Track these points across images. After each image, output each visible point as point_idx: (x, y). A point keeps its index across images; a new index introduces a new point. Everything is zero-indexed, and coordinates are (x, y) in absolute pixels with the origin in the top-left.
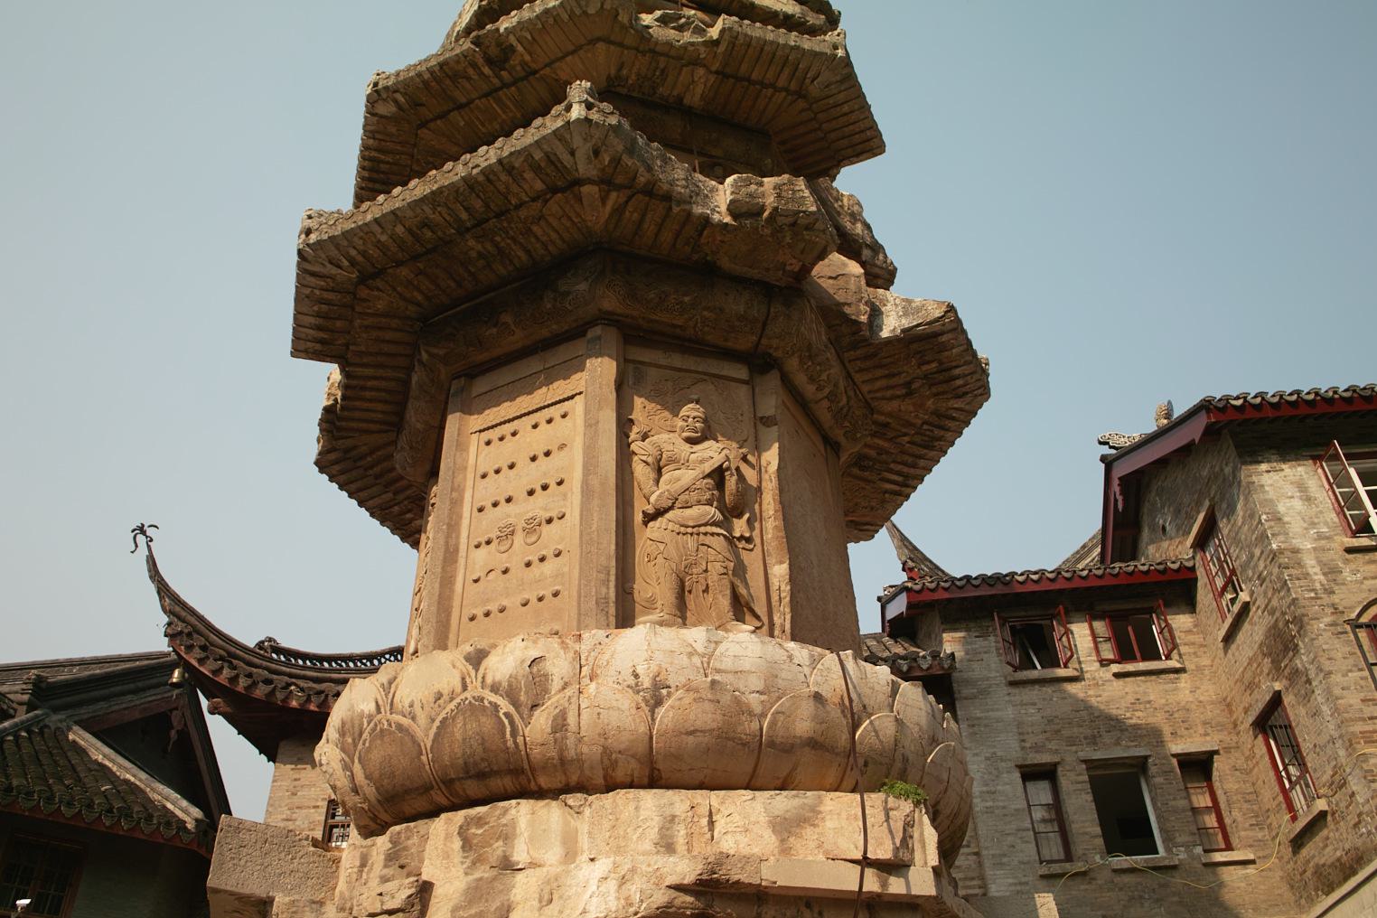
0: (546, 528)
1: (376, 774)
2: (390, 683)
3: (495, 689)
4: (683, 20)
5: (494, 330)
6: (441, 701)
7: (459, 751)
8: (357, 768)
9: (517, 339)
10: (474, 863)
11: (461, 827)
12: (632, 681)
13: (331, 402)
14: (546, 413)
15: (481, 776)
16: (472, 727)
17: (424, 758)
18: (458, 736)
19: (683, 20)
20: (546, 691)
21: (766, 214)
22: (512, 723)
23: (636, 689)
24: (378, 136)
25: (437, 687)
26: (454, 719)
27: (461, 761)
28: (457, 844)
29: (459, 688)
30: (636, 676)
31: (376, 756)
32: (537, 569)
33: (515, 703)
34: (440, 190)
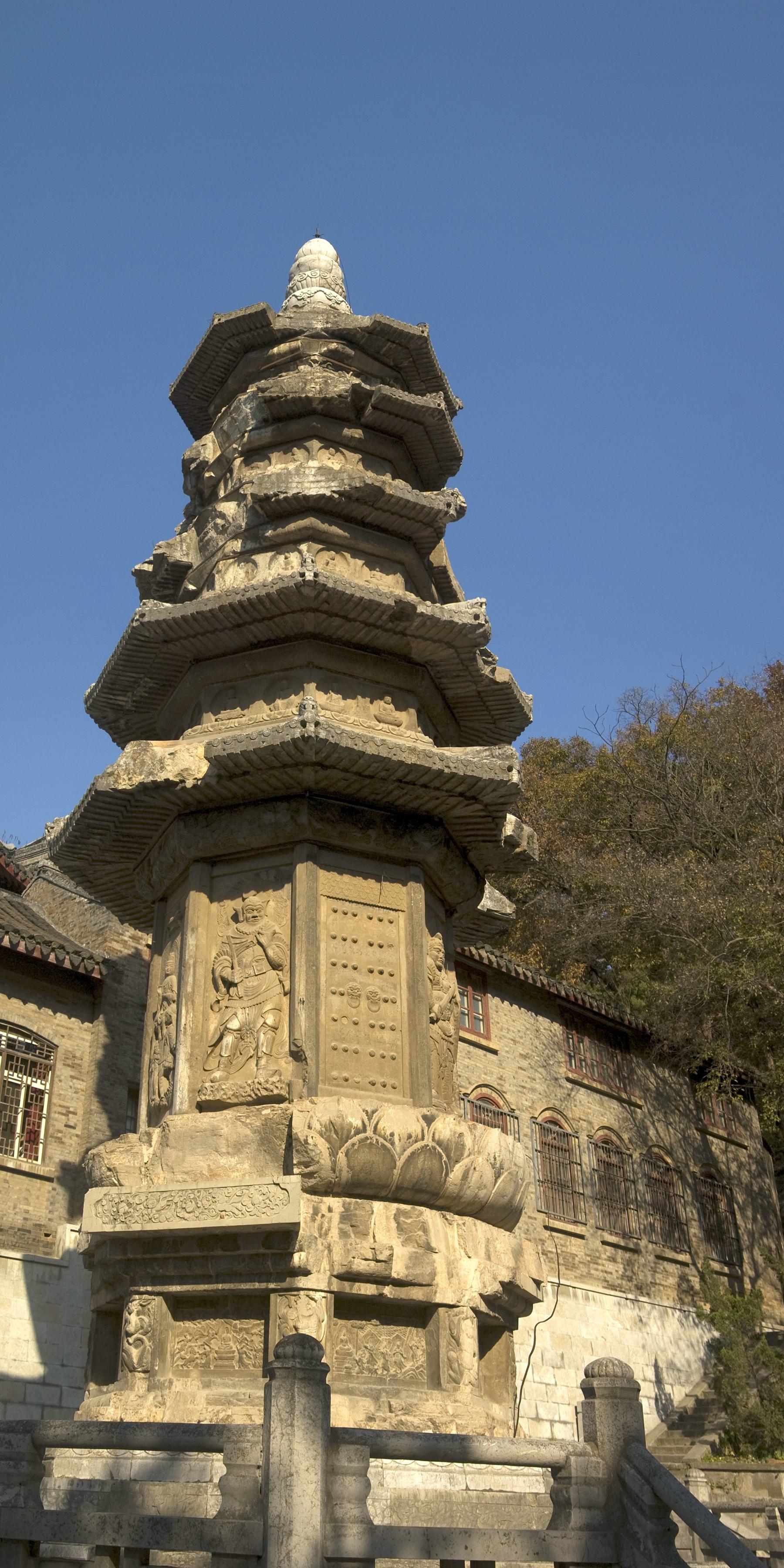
0: (383, 1005)
1: (358, 1168)
2: (374, 1112)
3: (439, 1143)
4: (490, 659)
5: (359, 835)
6: (411, 1140)
7: (417, 1175)
8: (341, 1156)
9: (370, 846)
10: (406, 1240)
11: (395, 1215)
12: (492, 1160)
13: (177, 780)
14: (371, 911)
15: (419, 1191)
16: (428, 1164)
17: (395, 1171)
18: (420, 1166)
19: (490, 659)
20: (462, 1154)
21: (518, 850)
22: (447, 1167)
23: (493, 1166)
24: (282, 596)
25: (410, 1130)
26: (419, 1155)
27: (415, 1180)
28: (394, 1225)
29: (420, 1136)
30: (495, 1159)
31: (363, 1157)
32: (377, 1033)
33: (448, 1157)
34: (420, 766)
